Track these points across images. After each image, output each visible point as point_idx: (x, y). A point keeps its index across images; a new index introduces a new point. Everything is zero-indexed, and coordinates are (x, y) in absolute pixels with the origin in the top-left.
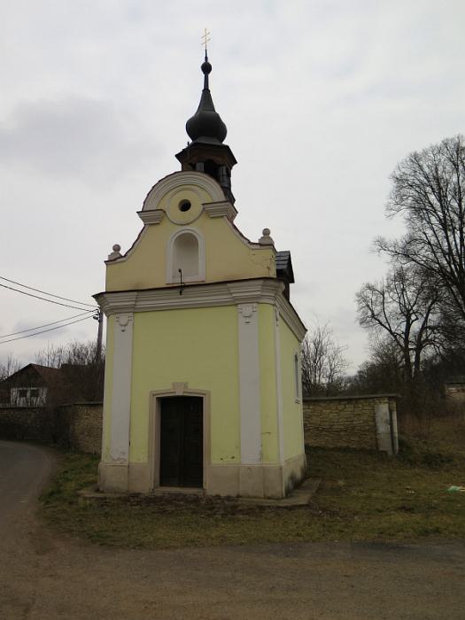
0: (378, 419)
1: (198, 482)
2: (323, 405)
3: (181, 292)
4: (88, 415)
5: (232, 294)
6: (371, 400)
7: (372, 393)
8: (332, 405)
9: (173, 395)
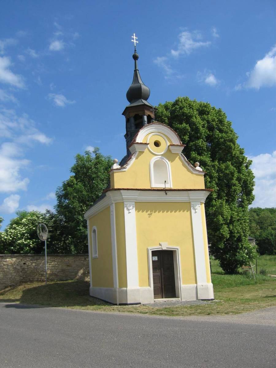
9: (161, 249)
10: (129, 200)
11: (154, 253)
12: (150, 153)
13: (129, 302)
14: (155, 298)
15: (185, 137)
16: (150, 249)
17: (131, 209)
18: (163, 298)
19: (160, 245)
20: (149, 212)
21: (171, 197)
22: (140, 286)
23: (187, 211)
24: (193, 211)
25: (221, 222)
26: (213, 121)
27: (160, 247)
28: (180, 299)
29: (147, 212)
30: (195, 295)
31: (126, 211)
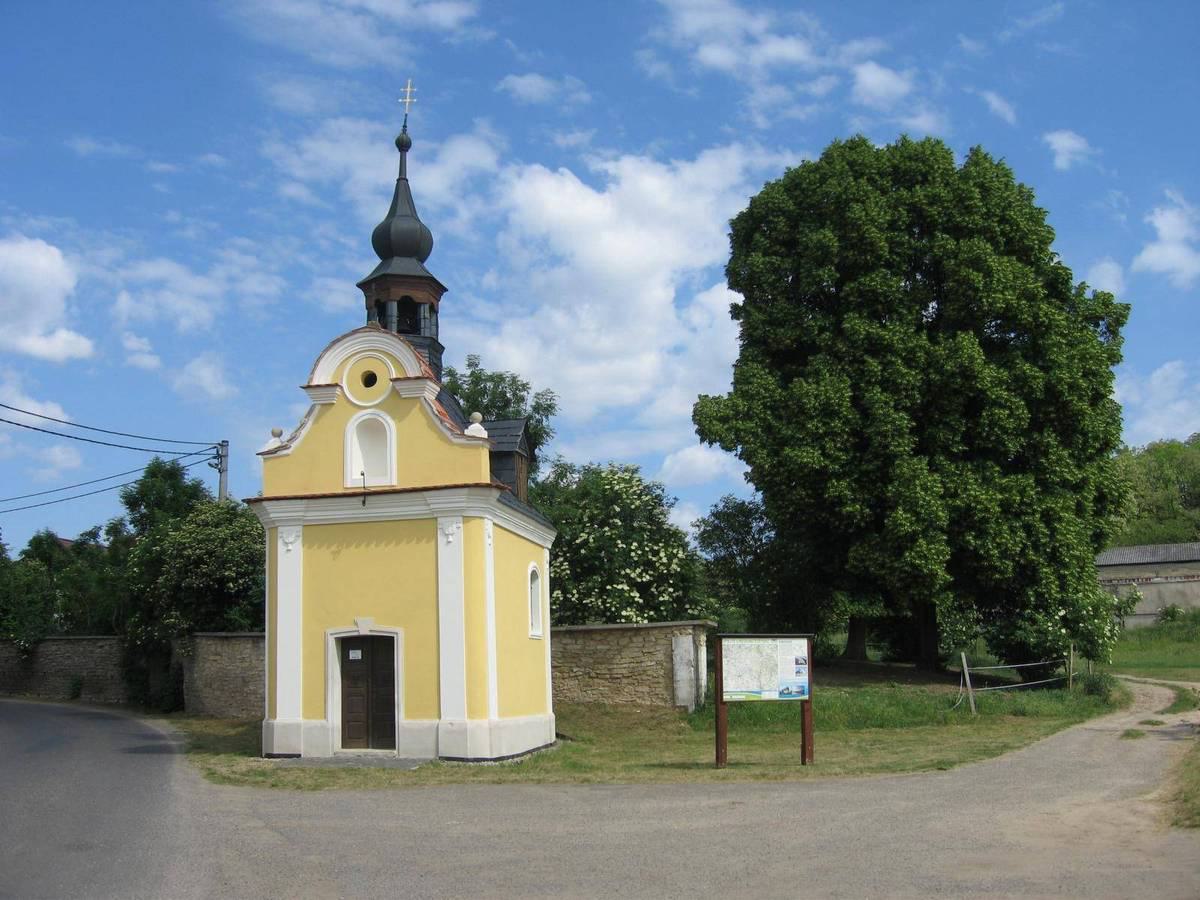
0: (677, 659)
1: (391, 744)
2: (598, 637)
3: (364, 502)
4: (217, 654)
5: (429, 505)
6: (669, 631)
7: (105, 634)
8: (610, 638)
9: (356, 634)
10: (289, 522)
11: (346, 644)
12: (348, 405)
13: (276, 752)
14: (343, 747)
15: (821, 272)
16: (331, 634)
17: (291, 543)
18: (368, 747)
19: (356, 624)
20: (334, 548)
21: (378, 509)
22: (306, 716)
23: (428, 542)
24: (441, 540)
25: (908, 528)
26: (931, 204)
27: (355, 628)
28: (395, 752)
29: (328, 548)
30: (432, 746)
31: (281, 548)
